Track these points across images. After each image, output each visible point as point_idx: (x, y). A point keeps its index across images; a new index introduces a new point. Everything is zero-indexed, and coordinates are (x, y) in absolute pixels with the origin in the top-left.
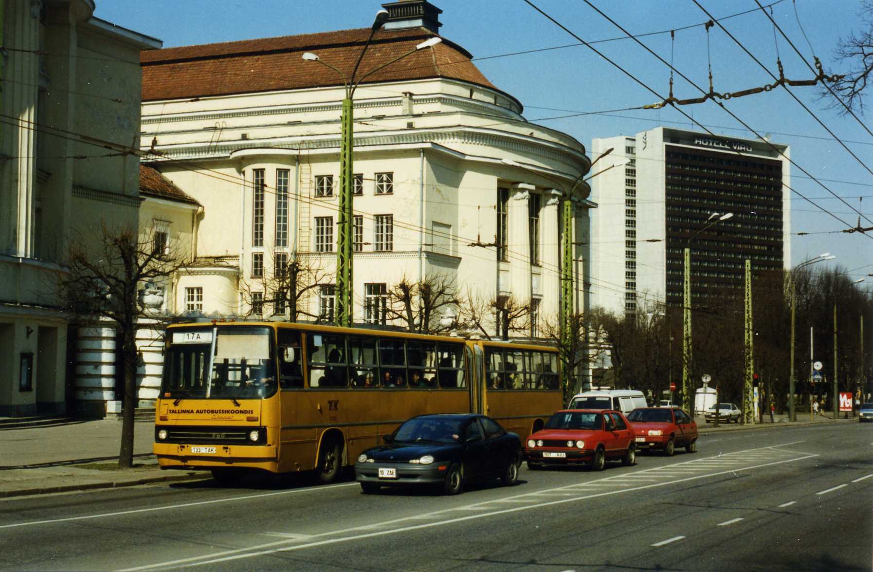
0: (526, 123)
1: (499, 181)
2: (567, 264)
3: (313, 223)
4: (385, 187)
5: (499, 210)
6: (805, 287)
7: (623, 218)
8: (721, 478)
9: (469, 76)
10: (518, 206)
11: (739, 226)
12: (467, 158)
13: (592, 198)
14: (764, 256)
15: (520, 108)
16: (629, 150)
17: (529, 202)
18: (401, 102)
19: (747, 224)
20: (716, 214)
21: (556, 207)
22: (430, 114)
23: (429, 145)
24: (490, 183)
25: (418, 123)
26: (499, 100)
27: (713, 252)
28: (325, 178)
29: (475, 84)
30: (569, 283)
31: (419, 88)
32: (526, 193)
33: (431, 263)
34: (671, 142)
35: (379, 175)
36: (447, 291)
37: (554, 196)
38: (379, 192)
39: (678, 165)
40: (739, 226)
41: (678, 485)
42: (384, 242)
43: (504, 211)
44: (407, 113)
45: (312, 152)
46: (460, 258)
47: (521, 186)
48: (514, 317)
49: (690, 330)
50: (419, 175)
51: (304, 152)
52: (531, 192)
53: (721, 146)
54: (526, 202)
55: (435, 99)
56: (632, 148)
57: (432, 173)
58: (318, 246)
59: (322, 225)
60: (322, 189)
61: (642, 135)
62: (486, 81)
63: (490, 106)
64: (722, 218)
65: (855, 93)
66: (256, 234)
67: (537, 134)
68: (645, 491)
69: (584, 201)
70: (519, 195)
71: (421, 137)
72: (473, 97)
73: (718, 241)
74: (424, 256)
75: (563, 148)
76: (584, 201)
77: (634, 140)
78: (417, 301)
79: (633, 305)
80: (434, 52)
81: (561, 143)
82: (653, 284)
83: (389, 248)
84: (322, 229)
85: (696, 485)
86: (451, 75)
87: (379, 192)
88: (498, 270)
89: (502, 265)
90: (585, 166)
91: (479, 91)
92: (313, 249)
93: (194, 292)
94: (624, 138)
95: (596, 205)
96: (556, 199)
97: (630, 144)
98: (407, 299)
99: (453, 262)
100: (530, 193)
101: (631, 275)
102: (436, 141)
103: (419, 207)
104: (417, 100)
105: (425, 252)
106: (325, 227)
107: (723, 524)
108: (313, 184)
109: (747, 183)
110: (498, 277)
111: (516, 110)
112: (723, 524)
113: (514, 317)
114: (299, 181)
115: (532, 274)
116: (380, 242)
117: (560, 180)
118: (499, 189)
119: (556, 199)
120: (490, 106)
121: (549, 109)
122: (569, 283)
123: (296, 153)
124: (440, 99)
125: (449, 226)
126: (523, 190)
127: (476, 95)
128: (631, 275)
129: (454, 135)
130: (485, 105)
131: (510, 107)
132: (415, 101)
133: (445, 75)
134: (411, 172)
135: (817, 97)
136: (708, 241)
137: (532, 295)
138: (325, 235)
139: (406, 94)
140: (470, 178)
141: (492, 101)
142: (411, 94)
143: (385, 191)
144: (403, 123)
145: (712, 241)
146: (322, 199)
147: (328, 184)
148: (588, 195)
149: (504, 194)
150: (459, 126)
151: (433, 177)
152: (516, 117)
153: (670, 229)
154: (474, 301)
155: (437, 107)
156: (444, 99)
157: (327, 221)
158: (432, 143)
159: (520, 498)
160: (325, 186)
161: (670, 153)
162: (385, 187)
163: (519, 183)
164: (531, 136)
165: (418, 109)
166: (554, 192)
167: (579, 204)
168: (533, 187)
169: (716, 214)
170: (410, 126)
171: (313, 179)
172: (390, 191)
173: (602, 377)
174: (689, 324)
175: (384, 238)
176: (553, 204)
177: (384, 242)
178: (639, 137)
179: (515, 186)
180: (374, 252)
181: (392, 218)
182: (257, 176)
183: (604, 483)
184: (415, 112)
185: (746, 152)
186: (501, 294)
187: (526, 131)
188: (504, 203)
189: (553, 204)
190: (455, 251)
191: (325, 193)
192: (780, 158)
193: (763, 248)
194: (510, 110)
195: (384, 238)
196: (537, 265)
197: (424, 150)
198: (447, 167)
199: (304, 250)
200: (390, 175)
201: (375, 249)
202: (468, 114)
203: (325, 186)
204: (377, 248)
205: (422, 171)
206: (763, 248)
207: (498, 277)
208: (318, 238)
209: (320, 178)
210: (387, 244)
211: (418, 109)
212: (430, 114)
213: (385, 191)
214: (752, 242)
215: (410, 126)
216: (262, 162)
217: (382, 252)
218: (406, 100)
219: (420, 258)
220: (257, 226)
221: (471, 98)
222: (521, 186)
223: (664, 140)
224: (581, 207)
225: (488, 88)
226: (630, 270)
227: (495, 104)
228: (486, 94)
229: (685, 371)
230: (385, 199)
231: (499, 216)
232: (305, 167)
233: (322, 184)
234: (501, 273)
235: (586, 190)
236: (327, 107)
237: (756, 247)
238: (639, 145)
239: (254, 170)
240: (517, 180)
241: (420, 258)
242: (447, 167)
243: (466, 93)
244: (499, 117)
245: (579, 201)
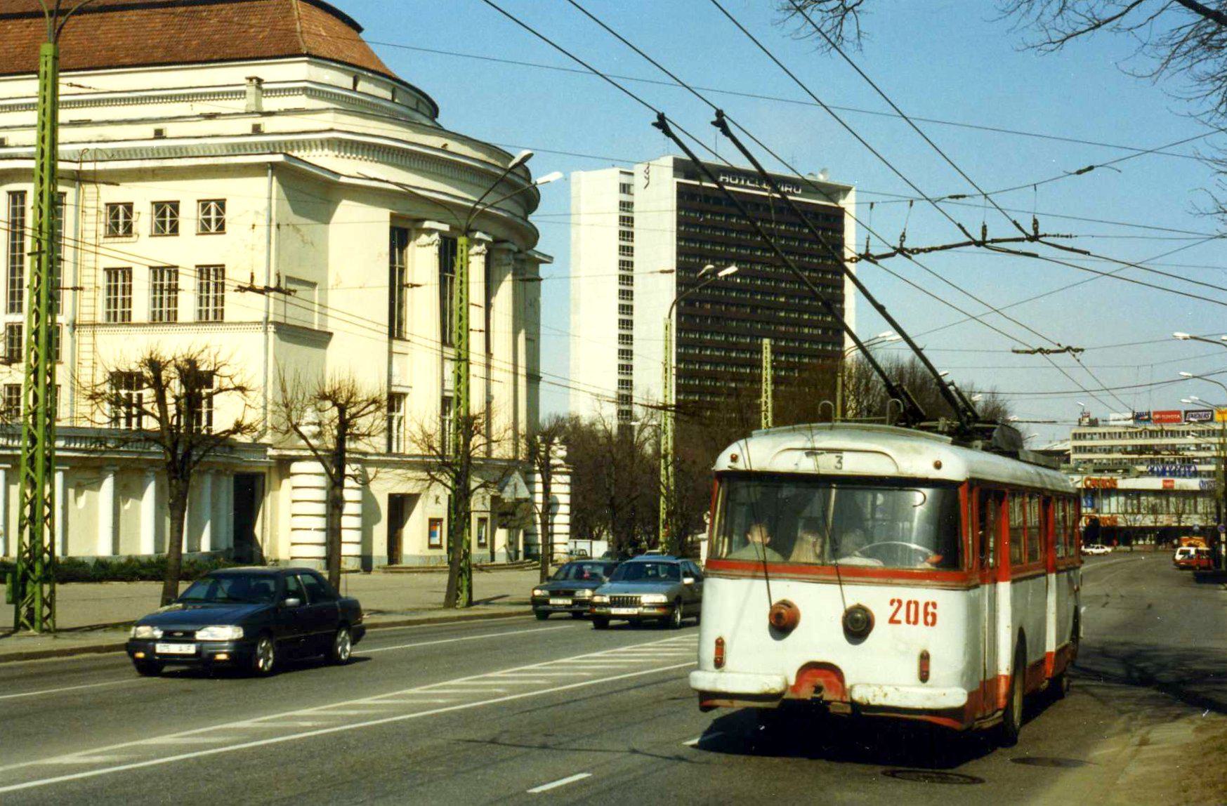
0: (439, 130)
1: (392, 216)
2: (460, 337)
3: (102, 279)
4: (213, 224)
5: (392, 261)
6: (867, 384)
7: (615, 287)
8: (563, 699)
9: (353, 55)
10: (422, 259)
11: (782, 299)
12: (343, 180)
13: (541, 247)
14: (817, 342)
15: (434, 110)
16: (625, 188)
17: (440, 250)
18: (245, 93)
19: (793, 297)
20: (710, 267)
21: (482, 259)
22: (287, 112)
23: (279, 158)
24: (378, 220)
25: (268, 124)
26: (399, 93)
27: (744, 336)
28: (121, 207)
29: (357, 69)
30: (464, 364)
31: (273, 72)
32: (436, 236)
33: (281, 339)
34: (687, 177)
35: (205, 204)
36: (221, 371)
37: (479, 242)
38: (205, 229)
39: (695, 211)
40: (782, 299)
41: (459, 714)
42: (211, 308)
43: (401, 262)
44: (253, 109)
45: (100, 166)
46: (331, 334)
47: (427, 224)
48: (354, 416)
49: (670, 444)
50: (265, 203)
51: (87, 167)
52: (442, 234)
53: (748, 183)
54: (435, 249)
55: (298, 89)
56: (629, 186)
57: (286, 203)
58: (109, 313)
59: (116, 280)
60: (117, 225)
61: (643, 167)
62: (382, 65)
63: (384, 104)
64: (721, 274)
65: (846, 10)
66: (13, 294)
67: (454, 146)
68: (534, 700)
69: (530, 252)
70: (424, 239)
71: (272, 148)
72: (359, 88)
73: (752, 321)
74: (271, 328)
75: (493, 170)
76: (530, 252)
77: (632, 174)
78: (176, 388)
79: (629, 413)
80: (299, 19)
81: (492, 161)
82: (655, 381)
83: (219, 317)
84: (116, 287)
85: (601, 692)
86: (325, 54)
87: (205, 229)
88: (391, 353)
89: (397, 346)
90: (530, 199)
91: (370, 80)
92: (101, 318)
93: (734, 459)
94: (616, 170)
95: (549, 259)
96: (483, 247)
97: (625, 179)
98: (160, 388)
99: (320, 339)
100: (441, 236)
101: (626, 369)
102: (295, 154)
103: (265, 254)
104: (271, 91)
105: (273, 323)
106: (120, 283)
107: (537, 790)
108: (102, 217)
109: (793, 239)
110: (390, 363)
111: (428, 113)
112: (537, 790)
113: (354, 416)
114: (80, 210)
115: (443, 359)
116: (204, 308)
117: (491, 222)
118: (393, 229)
119: (483, 247)
120: (384, 104)
121: (477, 113)
122: (464, 364)
123: (75, 167)
124: (305, 90)
125: (313, 285)
126: (430, 231)
127: (363, 86)
128: (626, 369)
129: (324, 144)
130: (375, 101)
131: (420, 108)
132: (267, 91)
133: (314, 53)
134: (252, 199)
135: (781, 16)
136: (738, 320)
137: (443, 390)
138: (120, 296)
139: (251, 79)
140: (347, 210)
141: (388, 95)
142: (260, 81)
143: (213, 229)
144: (246, 125)
145: (743, 321)
146: (117, 239)
147: (126, 216)
148: (535, 243)
149: (400, 237)
150: (331, 130)
151: (287, 207)
152: (429, 123)
153: (682, 304)
154: (289, 390)
155: (302, 101)
156: (311, 90)
157: (124, 273)
158: (285, 154)
159: (334, 709)
160: (121, 220)
161: (684, 194)
162: (213, 224)
163: (424, 220)
164: (444, 149)
165: (269, 104)
166: (478, 235)
167: (522, 256)
168: (445, 227)
169: (710, 267)
170: (257, 130)
171: (102, 207)
172: (221, 228)
173: (513, 514)
174: (670, 434)
175: (211, 301)
176: (478, 254)
177: (211, 308)
178: (639, 169)
179: (418, 225)
180: (196, 323)
181: (223, 271)
182: (14, 202)
183: (412, 696)
184: (266, 109)
185: (793, 194)
186: (394, 389)
187: (436, 141)
188: (401, 252)
189: (478, 254)
190: (322, 323)
191: (121, 231)
192: (842, 203)
193: (815, 332)
194: (417, 110)
195: (211, 301)
196: (401, 338)
197: (274, 166)
198: (310, 193)
199: (86, 318)
200: (221, 204)
201: (197, 319)
202: (346, 112)
203: (121, 220)
204: (200, 317)
205: (270, 198)
206: (815, 332)
207: (390, 363)
208: (109, 300)
209: (113, 207)
210: (215, 311)
211: (269, 104)
212: (287, 112)
213: (213, 229)
214: (800, 324)
215: (257, 130)
216: (20, 181)
217: (207, 322)
218: (251, 89)
219: (266, 331)
220: (13, 282)
221: (354, 89)
222: (427, 224)
223: (675, 176)
224: (523, 261)
225: (383, 76)
226: (625, 362)
227: (393, 101)
228: (378, 84)
229: (663, 506)
230: (213, 240)
231: (392, 270)
232: (89, 189)
233: (117, 216)
234: (395, 357)
235: (532, 236)
236: (120, 100)
237: (806, 330)
238: (638, 181)
239: (10, 193)
240: (424, 216)
241: (266, 331)
242: (310, 193)
243: (347, 81)
244: (394, 118)
245: (520, 252)
